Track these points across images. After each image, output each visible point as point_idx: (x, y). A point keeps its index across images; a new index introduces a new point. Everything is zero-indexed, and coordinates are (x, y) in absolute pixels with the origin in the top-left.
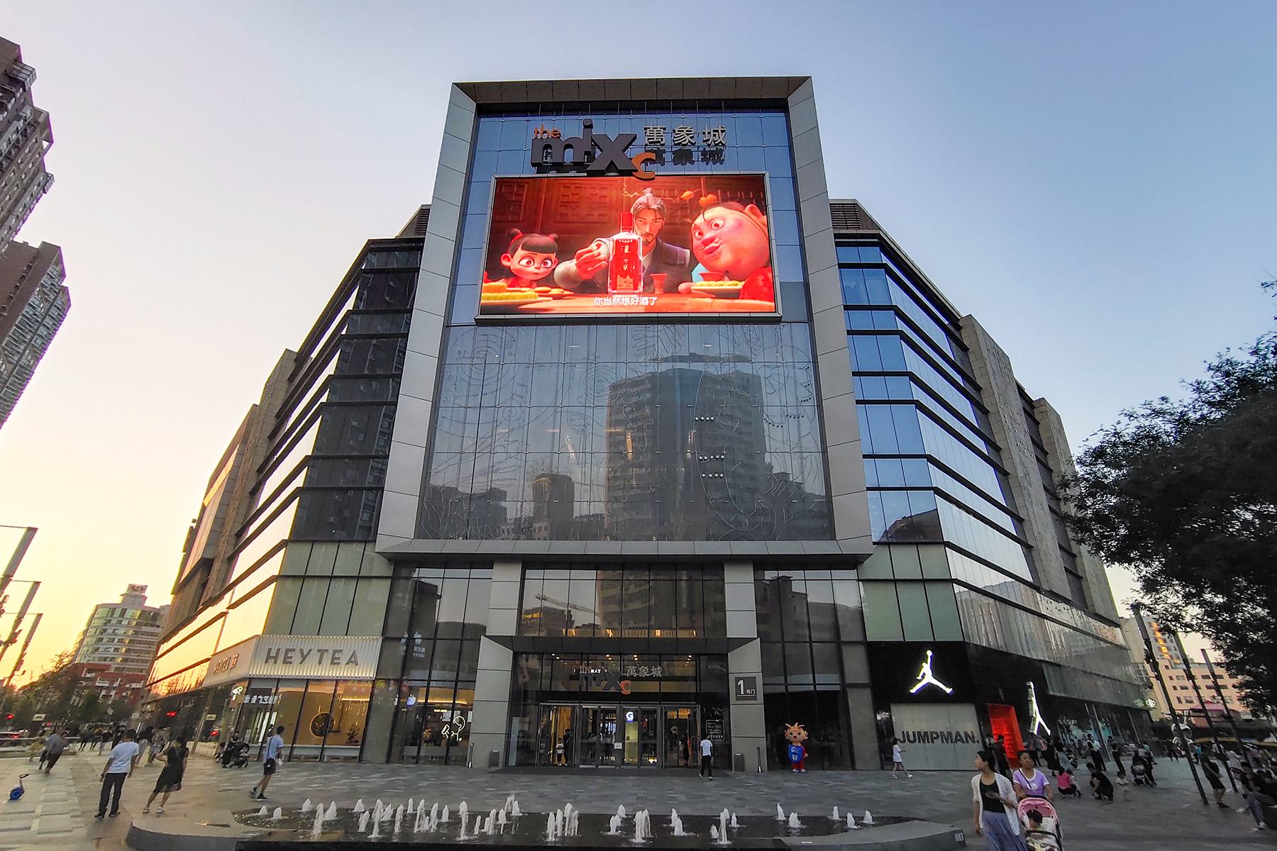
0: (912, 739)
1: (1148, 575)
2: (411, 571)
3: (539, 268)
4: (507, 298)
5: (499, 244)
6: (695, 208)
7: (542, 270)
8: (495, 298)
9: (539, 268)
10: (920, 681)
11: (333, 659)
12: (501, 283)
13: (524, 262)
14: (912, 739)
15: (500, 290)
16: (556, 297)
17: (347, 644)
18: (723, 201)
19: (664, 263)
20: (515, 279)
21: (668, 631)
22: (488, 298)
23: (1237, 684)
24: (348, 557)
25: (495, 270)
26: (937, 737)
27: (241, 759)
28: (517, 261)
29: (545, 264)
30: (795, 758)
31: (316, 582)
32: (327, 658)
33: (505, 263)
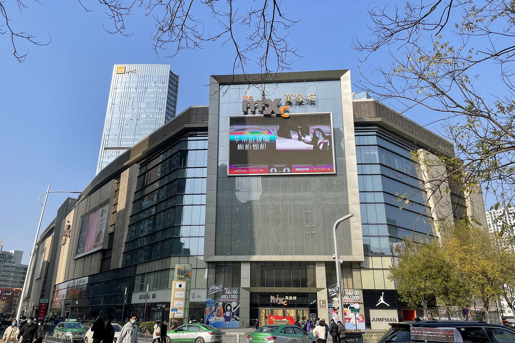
0: (376, 320)
10: (379, 302)
14: (376, 320)
21: (182, 306)
26: (384, 320)
31: (194, 269)
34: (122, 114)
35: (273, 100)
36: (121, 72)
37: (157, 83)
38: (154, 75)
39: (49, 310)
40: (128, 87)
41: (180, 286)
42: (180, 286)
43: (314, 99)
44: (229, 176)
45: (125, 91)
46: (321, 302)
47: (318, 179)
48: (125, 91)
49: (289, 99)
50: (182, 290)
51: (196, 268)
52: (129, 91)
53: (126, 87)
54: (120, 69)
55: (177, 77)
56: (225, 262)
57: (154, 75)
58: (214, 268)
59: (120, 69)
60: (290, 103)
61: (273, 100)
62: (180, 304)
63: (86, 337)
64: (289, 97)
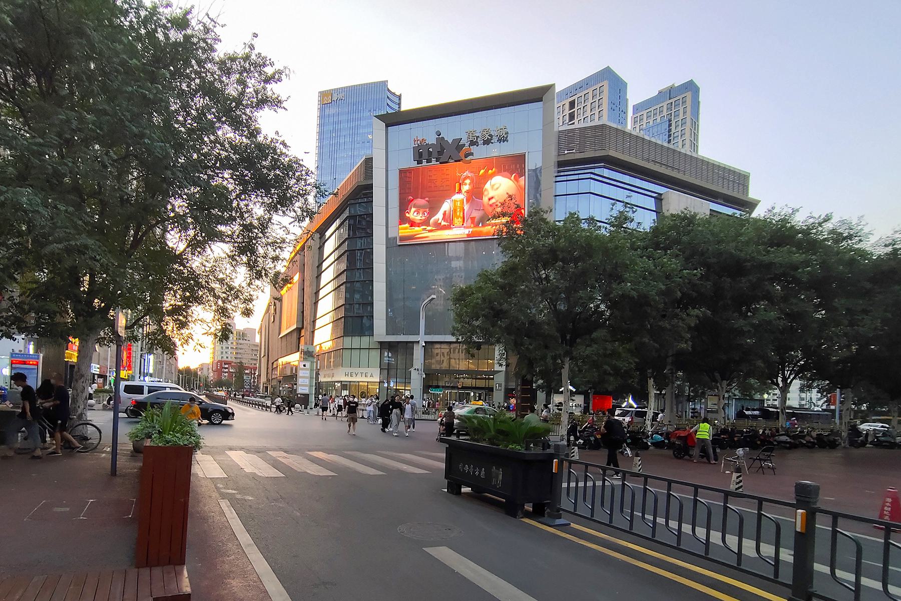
1: (218, 560)
2: (60, 345)
3: (421, 217)
4: (409, 232)
5: (404, 207)
6: (487, 178)
7: (423, 218)
8: (405, 233)
9: (421, 217)
11: (366, 375)
12: (407, 225)
13: (415, 213)
15: (406, 228)
16: (430, 231)
17: (369, 371)
18: (498, 173)
19: (475, 210)
20: (413, 224)
21: (308, 383)
22: (402, 233)
23: (189, 17)
24: (365, 341)
25: (403, 219)
27: (104, 455)
28: (412, 214)
29: (424, 214)
30: (511, 409)
31: (347, 350)
32: (364, 375)
33: (407, 215)
34: (333, 160)
35: (450, 142)
36: (327, 101)
37: (372, 110)
38: (367, 99)
39: (797, 525)
40: (337, 122)
41: (304, 366)
42: (304, 366)
43: (504, 134)
44: (399, 245)
45: (334, 128)
46: (497, 385)
47: (473, 243)
48: (334, 128)
49: (471, 138)
50: (307, 369)
51: (351, 349)
52: (339, 127)
53: (335, 123)
54: (326, 97)
55: (400, 97)
56: (398, 342)
57: (367, 99)
58: (379, 348)
59: (326, 97)
60: (473, 143)
61: (450, 142)
62: (305, 381)
63: (227, 415)
64: (471, 134)
